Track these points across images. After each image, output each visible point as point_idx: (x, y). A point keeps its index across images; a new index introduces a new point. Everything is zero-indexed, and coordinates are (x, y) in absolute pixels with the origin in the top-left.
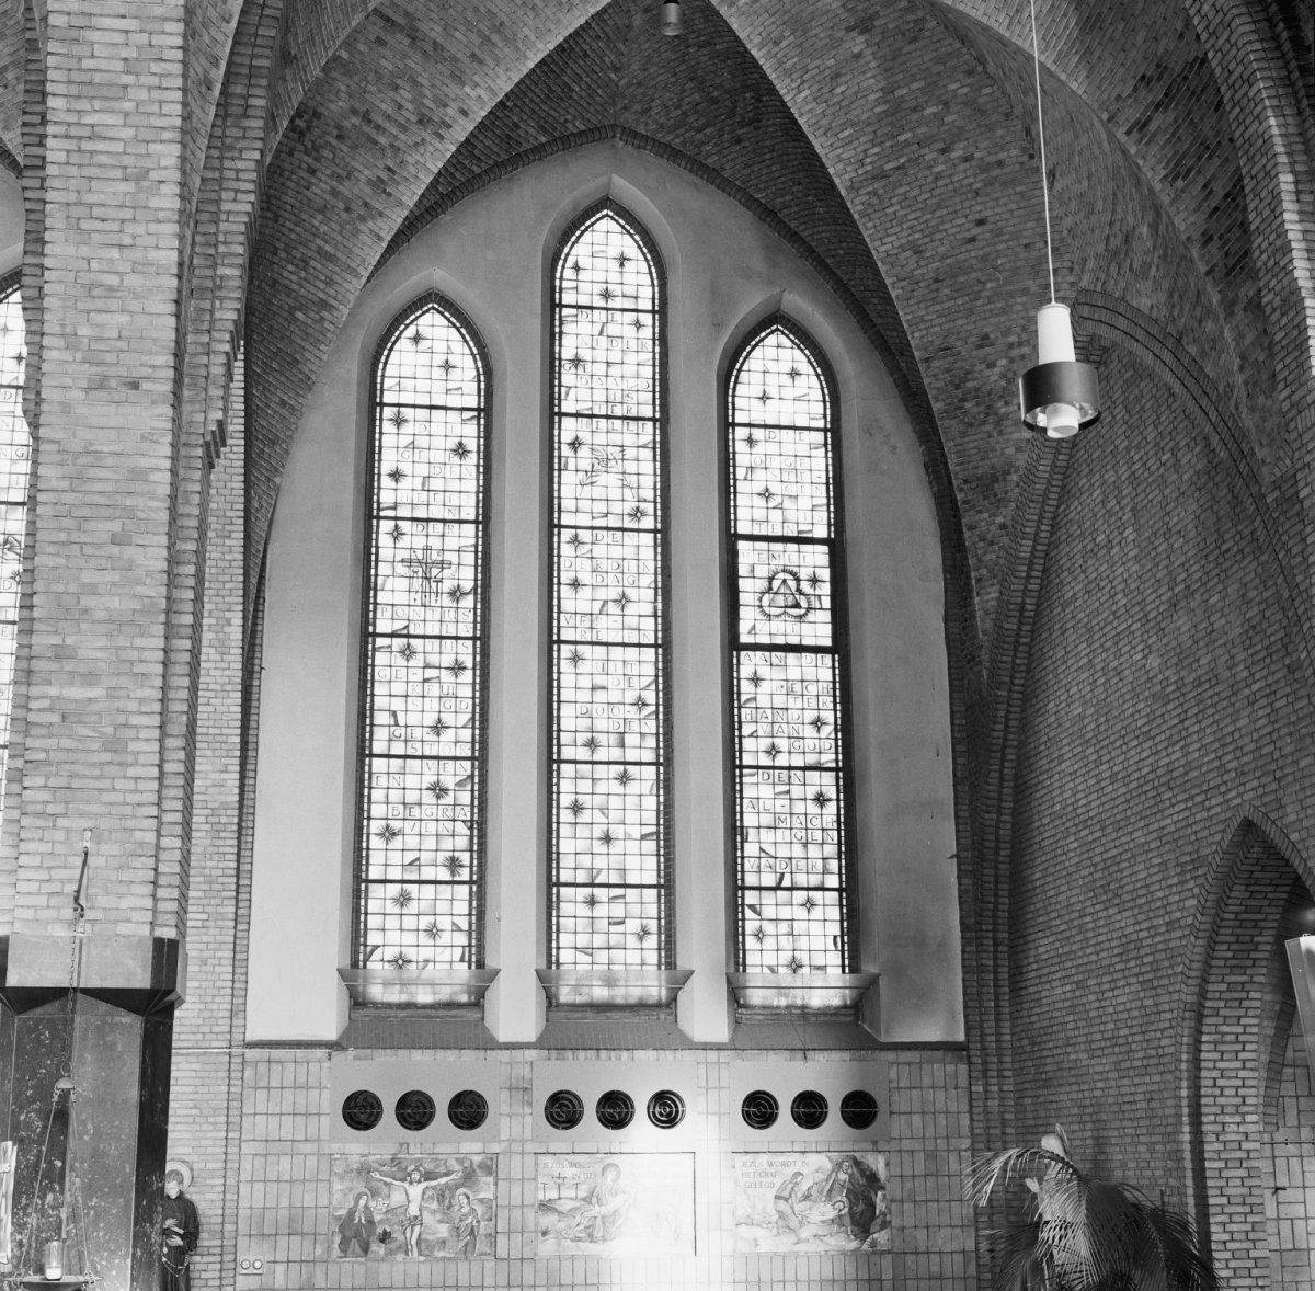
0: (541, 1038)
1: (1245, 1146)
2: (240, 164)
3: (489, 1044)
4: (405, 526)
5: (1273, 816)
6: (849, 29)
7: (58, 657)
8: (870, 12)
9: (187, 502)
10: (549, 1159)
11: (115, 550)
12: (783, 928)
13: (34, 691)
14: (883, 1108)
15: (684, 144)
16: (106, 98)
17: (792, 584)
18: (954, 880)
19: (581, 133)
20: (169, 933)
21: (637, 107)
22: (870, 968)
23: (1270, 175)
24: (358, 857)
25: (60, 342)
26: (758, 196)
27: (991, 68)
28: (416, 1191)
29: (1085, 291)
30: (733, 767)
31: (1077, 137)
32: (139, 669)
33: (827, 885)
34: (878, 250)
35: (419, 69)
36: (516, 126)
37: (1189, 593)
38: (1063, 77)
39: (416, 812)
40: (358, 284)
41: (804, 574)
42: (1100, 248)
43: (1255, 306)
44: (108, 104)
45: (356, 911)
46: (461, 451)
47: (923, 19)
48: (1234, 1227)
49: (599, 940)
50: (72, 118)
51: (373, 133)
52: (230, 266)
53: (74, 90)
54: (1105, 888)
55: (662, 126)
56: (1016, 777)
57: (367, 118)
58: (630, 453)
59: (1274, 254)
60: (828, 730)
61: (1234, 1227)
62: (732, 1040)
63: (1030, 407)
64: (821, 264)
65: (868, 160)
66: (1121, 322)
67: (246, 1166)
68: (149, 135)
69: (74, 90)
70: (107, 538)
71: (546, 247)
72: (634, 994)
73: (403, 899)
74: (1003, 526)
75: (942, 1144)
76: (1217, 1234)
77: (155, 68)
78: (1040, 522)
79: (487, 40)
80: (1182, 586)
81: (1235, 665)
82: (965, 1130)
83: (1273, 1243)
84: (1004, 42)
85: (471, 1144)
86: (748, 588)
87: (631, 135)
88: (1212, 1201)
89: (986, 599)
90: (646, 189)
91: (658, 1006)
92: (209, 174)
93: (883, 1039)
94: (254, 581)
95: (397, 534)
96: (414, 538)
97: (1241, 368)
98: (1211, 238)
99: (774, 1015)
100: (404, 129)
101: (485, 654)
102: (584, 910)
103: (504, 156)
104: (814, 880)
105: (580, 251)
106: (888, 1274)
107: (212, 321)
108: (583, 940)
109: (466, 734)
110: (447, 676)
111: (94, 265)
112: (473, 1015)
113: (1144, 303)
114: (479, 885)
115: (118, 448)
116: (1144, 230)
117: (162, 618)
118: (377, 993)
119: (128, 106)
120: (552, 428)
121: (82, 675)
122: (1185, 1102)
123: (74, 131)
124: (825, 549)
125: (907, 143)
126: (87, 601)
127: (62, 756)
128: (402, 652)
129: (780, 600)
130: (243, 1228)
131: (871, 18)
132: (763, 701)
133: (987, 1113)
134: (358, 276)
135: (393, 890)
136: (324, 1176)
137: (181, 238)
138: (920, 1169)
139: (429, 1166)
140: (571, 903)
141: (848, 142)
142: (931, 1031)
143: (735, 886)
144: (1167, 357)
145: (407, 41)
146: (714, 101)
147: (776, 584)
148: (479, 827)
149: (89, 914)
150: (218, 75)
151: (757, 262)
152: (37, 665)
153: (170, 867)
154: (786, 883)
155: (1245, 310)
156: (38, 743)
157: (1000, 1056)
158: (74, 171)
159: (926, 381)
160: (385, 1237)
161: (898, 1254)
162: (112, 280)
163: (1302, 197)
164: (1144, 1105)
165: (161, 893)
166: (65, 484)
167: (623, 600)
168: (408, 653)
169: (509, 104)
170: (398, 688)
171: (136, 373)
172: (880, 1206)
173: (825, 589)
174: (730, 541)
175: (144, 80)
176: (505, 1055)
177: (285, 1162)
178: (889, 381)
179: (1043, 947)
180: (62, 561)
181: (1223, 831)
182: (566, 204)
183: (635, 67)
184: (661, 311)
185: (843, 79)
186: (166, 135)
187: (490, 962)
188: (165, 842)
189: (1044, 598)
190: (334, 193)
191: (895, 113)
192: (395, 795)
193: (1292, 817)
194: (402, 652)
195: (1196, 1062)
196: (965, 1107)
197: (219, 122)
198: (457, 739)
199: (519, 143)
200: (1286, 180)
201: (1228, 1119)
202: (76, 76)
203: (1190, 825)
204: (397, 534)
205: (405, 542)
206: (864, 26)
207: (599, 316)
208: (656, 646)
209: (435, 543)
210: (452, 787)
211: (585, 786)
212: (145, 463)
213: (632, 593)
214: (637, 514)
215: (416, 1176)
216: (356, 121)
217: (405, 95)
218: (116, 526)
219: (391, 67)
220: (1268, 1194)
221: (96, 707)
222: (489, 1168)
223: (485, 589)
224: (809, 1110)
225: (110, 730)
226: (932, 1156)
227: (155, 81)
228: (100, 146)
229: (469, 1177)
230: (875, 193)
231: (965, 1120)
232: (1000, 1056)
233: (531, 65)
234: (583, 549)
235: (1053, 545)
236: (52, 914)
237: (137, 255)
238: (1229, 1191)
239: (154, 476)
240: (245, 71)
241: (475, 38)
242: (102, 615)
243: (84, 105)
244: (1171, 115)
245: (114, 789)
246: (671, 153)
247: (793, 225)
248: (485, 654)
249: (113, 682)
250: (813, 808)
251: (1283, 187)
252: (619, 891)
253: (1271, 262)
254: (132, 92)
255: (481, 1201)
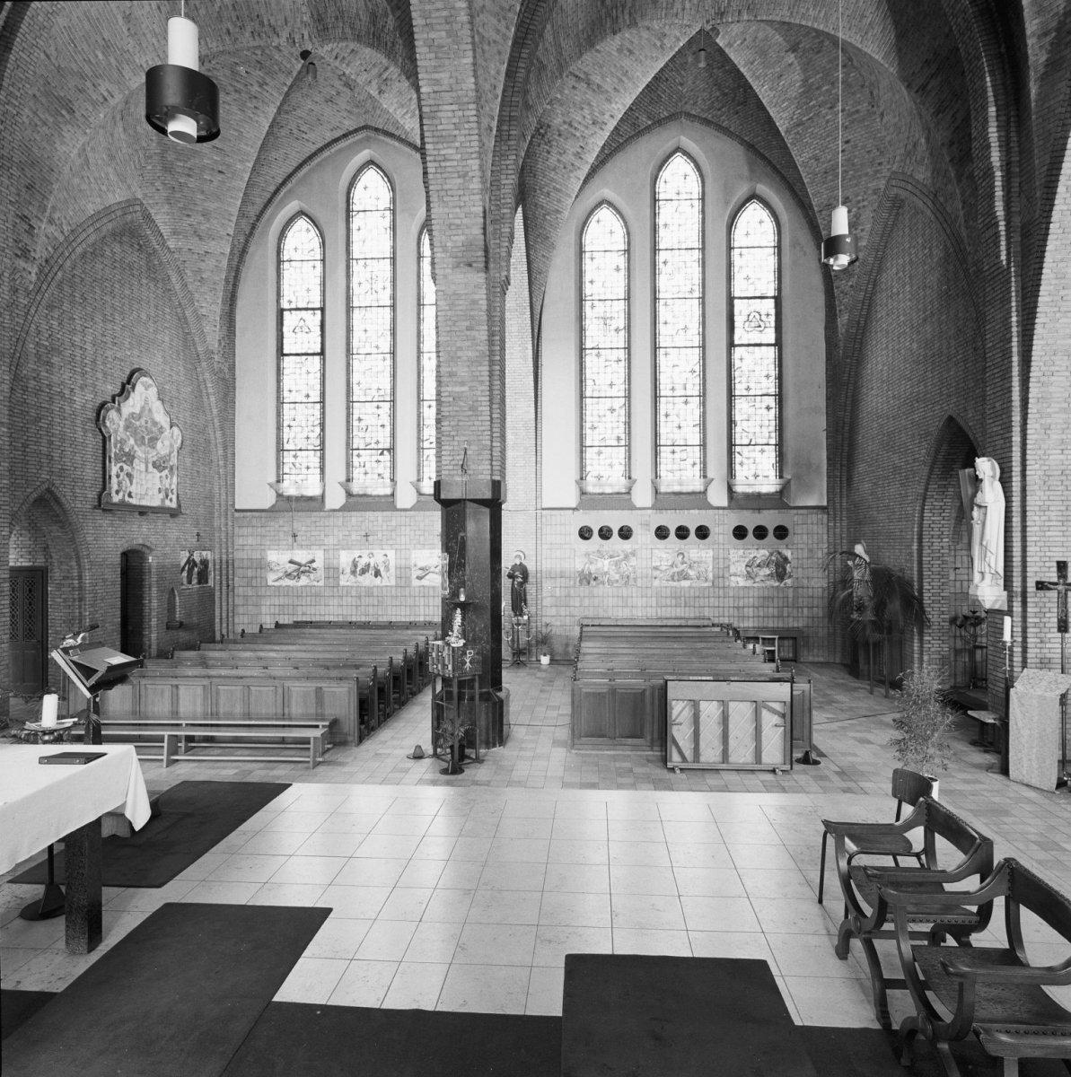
0: (653, 505)
1: (942, 551)
2: (508, 162)
3: (633, 508)
4: (596, 303)
5: (962, 415)
6: (786, 51)
7: (450, 376)
8: (797, 41)
9: (495, 311)
10: (657, 551)
11: (468, 333)
12: (752, 460)
13: (443, 389)
14: (791, 531)
15: (713, 117)
16: (448, 142)
17: (758, 317)
18: (825, 441)
19: (667, 117)
20: (497, 478)
21: (691, 102)
22: (787, 476)
23: (985, 108)
24: (582, 437)
25: (440, 250)
26: (746, 139)
27: (855, 63)
28: (606, 562)
29: (894, 173)
30: (731, 396)
31: (894, 94)
32: (480, 379)
33: (770, 443)
34: (798, 160)
35: (591, 98)
36: (638, 118)
37: (932, 314)
38: (887, 66)
39: (603, 419)
40: (570, 201)
41: (763, 313)
42: (902, 151)
43: (971, 177)
44: (449, 145)
45: (582, 458)
46: (618, 269)
47: (823, 41)
48: (934, 584)
49: (676, 467)
50: (436, 153)
51: (573, 131)
52: (506, 208)
53: (436, 140)
54: (888, 444)
55: (702, 110)
56: (853, 396)
57: (570, 125)
58: (688, 265)
59: (982, 149)
60: (772, 379)
61: (934, 584)
62: (729, 506)
63: (826, 257)
64: (774, 168)
65: (795, 117)
66: (910, 187)
67: (544, 552)
68: (466, 156)
69: (436, 140)
70: (464, 328)
71: (652, 174)
72: (690, 489)
73: (599, 453)
74: (852, 286)
75: (815, 546)
76: (926, 586)
77: (466, 126)
78: (868, 284)
79: (620, 80)
80: (929, 312)
81: (950, 347)
82: (825, 540)
83: (952, 590)
84: (860, 50)
85: (626, 545)
86: (739, 321)
87: (688, 115)
88: (925, 573)
89: (843, 320)
90: (695, 141)
91: (700, 493)
92: (494, 168)
93: (792, 505)
94: (536, 331)
95: (593, 307)
96: (600, 307)
97: (963, 208)
98: (953, 143)
99: (748, 496)
100: (587, 128)
101: (629, 354)
102: (671, 456)
103: (633, 133)
104: (765, 441)
105: (666, 174)
106: (791, 595)
107: (501, 233)
108: (670, 467)
109: (623, 387)
110: (614, 364)
111: (451, 216)
112: (626, 497)
113: (920, 177)
114: (629, 446)
115: (466, 292)
116: (923, 140)
117: (487, 358)
118: (590, 489)
119: (457, 144)
120: (655, 256)
121: (460, 383)
122: (915, 533)
123: (437, 158)
124: (773, 300)
125: (814, 106)
126: (459, 354)
127: (454, 413)
128: (597, 355)
129: (753, 324)
130: (544, 575)
131: (798, 44)
132: (744, 368)
133: (834, 534)
134: (570, 197)
135: (596, 449)
136: (572, 556)
137: (484, 201)
138: (805, 555)
139: (611, 553)
140: (665, 453)
141: (787, 108)
142: (812, 501)
143: (731, 445)
144: (930, 203)
145: (585, 86)
146: (725, 94)
147: (751, 317)
148: (628, 424)
149: (469, 472)
150: (494, 124)
151: (745, 171)
152: (442, 379)
153: (496, 453)
154: (753, 443)
155: (967, 178)
156: (446, 409)
157: (841, 512)
158: (439, 176)
159: (819, 221)
160: (595, 579)
161: (796, 588)
162: (458, 221)
163: (1000, 119)
164: (898, 534)
165: (494, 463)
166: (447, 308)
167: (685, 329)
168: (598, 355)
169: (634, 108)
170: (595, 370)
171: (470, 260)
172: (788, 569)
173: (772, 318)
174: (731, 300)
175: (463, 132)
176: (639, 512)
177: (558, 552)
178: (803, 221)
179: (861, 468)
180: (449, 339)
181: (939, 421)
182: (661, 154)
183: (689, 82)
184: (703, 199)
185: (784, 77)
186: (474, 156)
187: (633, 476)
188: (494, 444)
189: (868, 318)
190: (559, 161)
191: (808, 90)
192: (595, 413)
193: (970, 415)
194: (597, 355)
195: (922, 518)
196: (825, 531)
197: (498, 139)
198: (619, 390)
199: (639, 126)
200: (992, 110)
201: (935, 540)
202: (436, 134)
203: (925, 418)
204: (593, 307)
205: (596, 310)
206: (794, 49)
207: (675, 203)
208: (700, 347)
209: (608, 309)
210: (617, 408)
211: (670, 406)
212: (477, 297)
213: (689, 326)
214: (691, 291)
215: (606, 557)
216: (566, 126)
217: (586, 112)
218: (468, 323)
219: (579, 99)
220: (951, 571)
221: (465, 394)
222: (633, 554)
223: (629, 328)
224: (760, 533)
225: (471, 403)
226: (811, 551)
227: (467, 132)
228: (448, 164)
229: (626, 557)
230: (798, 133)
231: (825, 537)
232: (841, 512)
233: (640, 90)
234: (669, 308)
235: (874, 293)
236: (455, 472)
237: (466, 210)
238: (932, 569)
239: (481, 302)
240: (508, 119)
241: (615, 80)
242: (465, 358)
243: (440, 146)
244: (939, 79)
245: (474, 425)
246: (707, 122)
247: (762, 151)
248: (629, 354)
249: (470, 384)
250: (765, 411)
251: (990, 114)
252: (685, 448)
253: (980, 155)
254: (459, 139)
255: (631, 566)
